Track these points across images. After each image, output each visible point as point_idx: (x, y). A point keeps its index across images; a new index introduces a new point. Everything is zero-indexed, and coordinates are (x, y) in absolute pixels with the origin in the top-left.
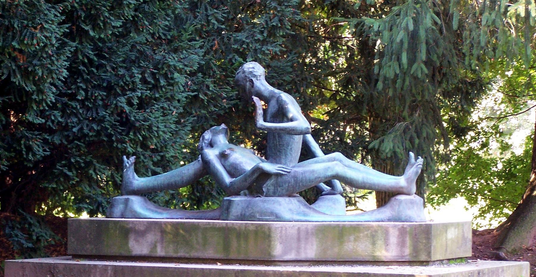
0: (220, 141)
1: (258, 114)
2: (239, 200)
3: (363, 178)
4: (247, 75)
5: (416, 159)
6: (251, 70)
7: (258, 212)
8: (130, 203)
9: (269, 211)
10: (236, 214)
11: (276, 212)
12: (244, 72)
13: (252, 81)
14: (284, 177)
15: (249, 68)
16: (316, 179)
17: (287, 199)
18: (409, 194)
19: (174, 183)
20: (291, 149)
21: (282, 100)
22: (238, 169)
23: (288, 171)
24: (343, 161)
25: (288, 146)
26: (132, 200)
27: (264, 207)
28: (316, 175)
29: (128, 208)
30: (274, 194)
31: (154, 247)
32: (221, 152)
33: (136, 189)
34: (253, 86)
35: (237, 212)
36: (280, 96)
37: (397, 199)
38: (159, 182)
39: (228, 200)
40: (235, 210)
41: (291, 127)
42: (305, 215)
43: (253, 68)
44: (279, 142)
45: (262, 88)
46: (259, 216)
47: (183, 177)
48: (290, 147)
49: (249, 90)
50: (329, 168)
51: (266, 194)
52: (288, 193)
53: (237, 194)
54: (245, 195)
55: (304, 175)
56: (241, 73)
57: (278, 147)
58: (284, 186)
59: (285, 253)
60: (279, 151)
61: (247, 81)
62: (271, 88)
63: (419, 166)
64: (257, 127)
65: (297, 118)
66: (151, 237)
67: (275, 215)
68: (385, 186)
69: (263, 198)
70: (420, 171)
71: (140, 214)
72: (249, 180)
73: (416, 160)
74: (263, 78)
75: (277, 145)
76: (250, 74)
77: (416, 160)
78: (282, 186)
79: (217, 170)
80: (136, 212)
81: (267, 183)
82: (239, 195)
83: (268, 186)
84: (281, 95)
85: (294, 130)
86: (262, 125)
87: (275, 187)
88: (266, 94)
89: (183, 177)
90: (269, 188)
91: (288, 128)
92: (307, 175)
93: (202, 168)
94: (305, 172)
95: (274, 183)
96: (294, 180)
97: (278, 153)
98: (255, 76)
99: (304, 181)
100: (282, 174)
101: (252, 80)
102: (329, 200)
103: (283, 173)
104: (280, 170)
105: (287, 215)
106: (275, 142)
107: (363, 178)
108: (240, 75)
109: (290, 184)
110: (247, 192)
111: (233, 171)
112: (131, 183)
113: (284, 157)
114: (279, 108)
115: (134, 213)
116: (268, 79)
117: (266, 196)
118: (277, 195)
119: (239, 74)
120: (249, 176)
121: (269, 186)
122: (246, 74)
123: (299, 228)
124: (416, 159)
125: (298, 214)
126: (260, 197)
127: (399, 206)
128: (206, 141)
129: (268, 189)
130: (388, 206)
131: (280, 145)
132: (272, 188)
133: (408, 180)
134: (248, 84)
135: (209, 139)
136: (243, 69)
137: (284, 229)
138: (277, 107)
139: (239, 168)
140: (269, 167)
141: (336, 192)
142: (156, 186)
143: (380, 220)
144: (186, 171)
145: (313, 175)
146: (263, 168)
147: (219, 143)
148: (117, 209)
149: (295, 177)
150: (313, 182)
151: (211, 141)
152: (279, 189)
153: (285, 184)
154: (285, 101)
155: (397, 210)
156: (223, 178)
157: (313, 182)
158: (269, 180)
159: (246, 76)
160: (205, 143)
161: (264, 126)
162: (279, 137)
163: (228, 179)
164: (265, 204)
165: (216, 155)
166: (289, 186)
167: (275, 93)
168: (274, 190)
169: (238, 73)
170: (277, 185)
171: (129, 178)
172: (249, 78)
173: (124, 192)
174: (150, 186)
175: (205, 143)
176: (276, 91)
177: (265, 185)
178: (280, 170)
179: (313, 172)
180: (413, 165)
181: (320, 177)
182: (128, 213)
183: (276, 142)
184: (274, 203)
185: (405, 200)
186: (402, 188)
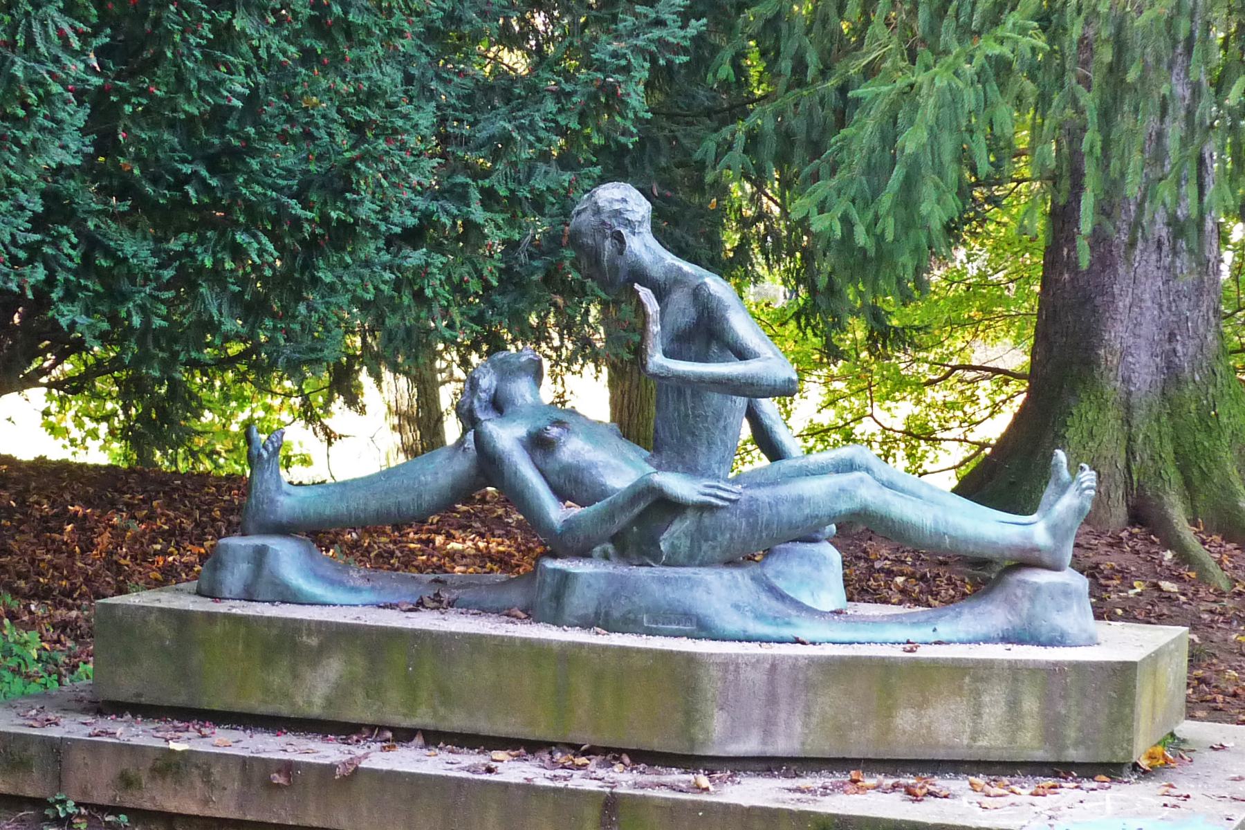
0: (523, 396)
1: (651, 335)
2: (590, 575)
3: (936, 522)
4: (607, 220)
5: (1075, 468)
6: (617, 206)
7: (648, 611)
8: (270, 560)
9: (680, 610)
10: (581, 612)
11: (699, 611)
12: (598, 211)
13: (619, 238)
14: (720, 514)
15: (611, 202)
16: (807, 518)
17: (727, 573)
18: (1055, 567)
19: (698, 707)
20: (725, 427)
21: (710, 294)
22: (582, 483)
23: (733, 497)
24: (875, 470)
25: (718, 421)
26: (276, 553)
27: (665, 596)
28: (807, 511)
29: (266, 572)
30: (692, 559)
31: (341, 692)
32: (534, 431)
33: (285, 520)
34: (621, 252)
35: (587, 607)
36: (705, 284)
37: (1025, 582)
38: (353, 505)
39: (559, 571)
40: (580, 600)
41: (744, 376)
42: (775, 620)
43: (624, 200)
44: (693, 408)
45: (647, 259)
46: (649, 622)
47: (420, 496)
48: (722, 423)
49: (612, 261)
50: (842, 490)
51: (669, 557)
52: (728, 556)
53: (584, 553)
54: (606, 557)
55: (774, 511)
56: (589, 212)
57: (691, 421)
58: (719, 539)
59: (733, 736)
60: (693, 434)
61: (605, 237)
62: (670, 259)
63: (1087, 492)
64: (645, 371)
65: (757, 349)
66: (333, 668)
67: (694, 620)
68: (995, 543)
69: (658, 570)
70: (1089, 506)
71: (299, 590)
72: (622, 520)
73: (1073, 475)
74: (646, 228)
75: (687, 416)
76: (615, 217)
77: (1073, 475)
78: (715, 538)
79: (524, 480)
80: (287, 587)
81: (673, 528)
82: (590, 556)
83: (674, 535)
84: (707, 280)
85: (752, 384)
86: (662, 367)
87: (692, 540)
88: (656, 272)
89: (420, 496)
90: (676, 542)
91: (737, 378)
92: (784, 509)
93: (473, 472)
94: (778, 501)
95: (693, 528)
96: (748, 524)
97: (689, 439)
98: (629, 223)
99: (775, 526)
100: (717, 507)
101: (619, 232)
102: (801, 557)
103: (720, 503)
104: (710, 495)
105: (732, 622)
106: (682, 408)
107: (936, 522)
108: (584, 220)
109: (735, 535)
110: (610, 548)
111: (569, 487)
112: (272, 501)
113: (704, 449)
114: (700, 316)
115: (279, 589)
116: (657, 232)
117: (665, 564)
118: (697, 562)
119: (583, 216)
120: (623, 509)
121: (678, 538)
122: (604, 217)
123: (774, 667)
124: (1075, 468)
125: (759, 617)
126: (651, 566)
127: (1032, 600)
128: (483, 395)
129: (672, 544)
130: (998, 596)
131: (695, 416)
132: (684, 545)
133: (1054, 530)
134: (608, 243)
135: (489, 389)
136: (596, 203)
137: (732, 668)
138: (692, 313)
139: (587, 481)
140: (678, 485)
141: (820, 536)
142: (342, 515)
143: (980, 636)
144: (429, 478)
145: (799, 508)
146: (665, 489)
147: (519, 402)
148: (233, 573)
149: (751, 514)
150: (798, 527)
151: (496, 391)
152: (705, 547)
153: (722, 534)
154: (719, 301)
155: (1025, 611)
156: (541, 507)
157: (798, 527)
158: (678, 518)
159: (604, 223)
160: (479, 399)
161: (668, 370)
162: (693, 395)
163: (556, 512)
164: (668, 589)
165: (520, 440)
166: (732, 538)
167: (686, 274)
168: (692, 547)
169: (579, 213)
170: (699, 535)
171: (268, 489)
172: (611, 228)
173: (251, 526)
174: (327, 512)
175: (479, 399)
176: (687, 267)
177: (666, 535)
178: (710, 495)
179: (800, 500)
180: (1063, 489)
181: (817, 516)
182: (263, 589)
183: (687, 409)
184: (692, 586)
185: (1049, 584)
186: (1037, 549)
